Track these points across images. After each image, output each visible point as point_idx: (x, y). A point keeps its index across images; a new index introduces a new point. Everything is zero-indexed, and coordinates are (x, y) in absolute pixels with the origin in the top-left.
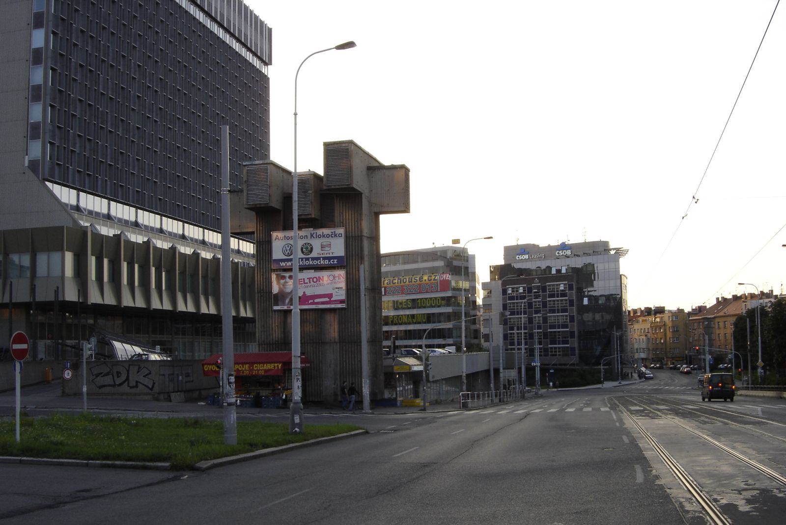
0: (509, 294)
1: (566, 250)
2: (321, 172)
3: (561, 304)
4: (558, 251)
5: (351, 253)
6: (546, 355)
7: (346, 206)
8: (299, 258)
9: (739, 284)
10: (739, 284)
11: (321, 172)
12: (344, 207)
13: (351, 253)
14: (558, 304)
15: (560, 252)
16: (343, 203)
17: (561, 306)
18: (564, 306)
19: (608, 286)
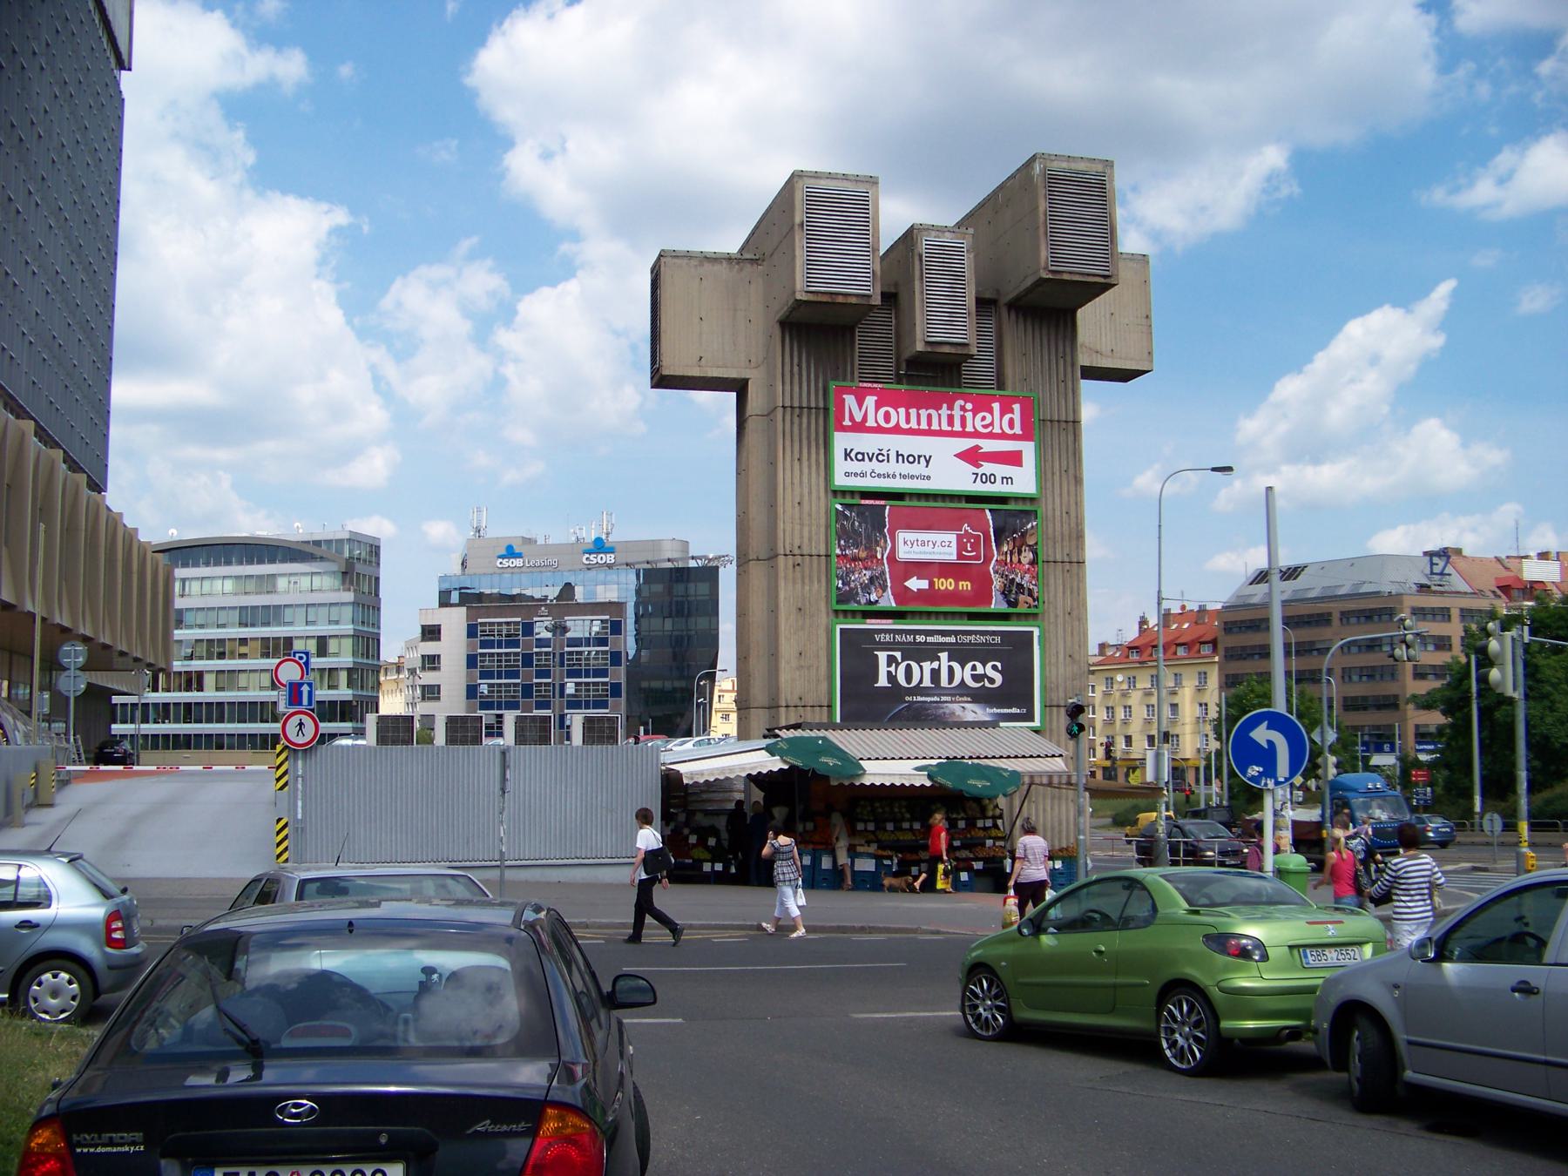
0: (569, 695)
1: (605, 553)
2: (876, 398)
3: (506, 661)
4: (587, 556)
5: (549, 762)
6: (224, 653)
7: (1057, 339)
8: (1003, 478)
9: (1229, 469)
10: (1229, 469)
11: (876, 398)
12: (1053, 338)
13: (549, 762)
14: (589, 690)
15: (592, 557)
16: (1049, 335)
17: (594, 696)
18: (600, 696)
19: (625, 581)
